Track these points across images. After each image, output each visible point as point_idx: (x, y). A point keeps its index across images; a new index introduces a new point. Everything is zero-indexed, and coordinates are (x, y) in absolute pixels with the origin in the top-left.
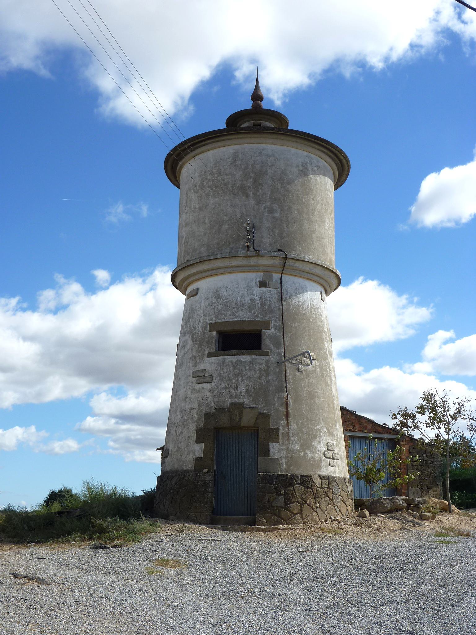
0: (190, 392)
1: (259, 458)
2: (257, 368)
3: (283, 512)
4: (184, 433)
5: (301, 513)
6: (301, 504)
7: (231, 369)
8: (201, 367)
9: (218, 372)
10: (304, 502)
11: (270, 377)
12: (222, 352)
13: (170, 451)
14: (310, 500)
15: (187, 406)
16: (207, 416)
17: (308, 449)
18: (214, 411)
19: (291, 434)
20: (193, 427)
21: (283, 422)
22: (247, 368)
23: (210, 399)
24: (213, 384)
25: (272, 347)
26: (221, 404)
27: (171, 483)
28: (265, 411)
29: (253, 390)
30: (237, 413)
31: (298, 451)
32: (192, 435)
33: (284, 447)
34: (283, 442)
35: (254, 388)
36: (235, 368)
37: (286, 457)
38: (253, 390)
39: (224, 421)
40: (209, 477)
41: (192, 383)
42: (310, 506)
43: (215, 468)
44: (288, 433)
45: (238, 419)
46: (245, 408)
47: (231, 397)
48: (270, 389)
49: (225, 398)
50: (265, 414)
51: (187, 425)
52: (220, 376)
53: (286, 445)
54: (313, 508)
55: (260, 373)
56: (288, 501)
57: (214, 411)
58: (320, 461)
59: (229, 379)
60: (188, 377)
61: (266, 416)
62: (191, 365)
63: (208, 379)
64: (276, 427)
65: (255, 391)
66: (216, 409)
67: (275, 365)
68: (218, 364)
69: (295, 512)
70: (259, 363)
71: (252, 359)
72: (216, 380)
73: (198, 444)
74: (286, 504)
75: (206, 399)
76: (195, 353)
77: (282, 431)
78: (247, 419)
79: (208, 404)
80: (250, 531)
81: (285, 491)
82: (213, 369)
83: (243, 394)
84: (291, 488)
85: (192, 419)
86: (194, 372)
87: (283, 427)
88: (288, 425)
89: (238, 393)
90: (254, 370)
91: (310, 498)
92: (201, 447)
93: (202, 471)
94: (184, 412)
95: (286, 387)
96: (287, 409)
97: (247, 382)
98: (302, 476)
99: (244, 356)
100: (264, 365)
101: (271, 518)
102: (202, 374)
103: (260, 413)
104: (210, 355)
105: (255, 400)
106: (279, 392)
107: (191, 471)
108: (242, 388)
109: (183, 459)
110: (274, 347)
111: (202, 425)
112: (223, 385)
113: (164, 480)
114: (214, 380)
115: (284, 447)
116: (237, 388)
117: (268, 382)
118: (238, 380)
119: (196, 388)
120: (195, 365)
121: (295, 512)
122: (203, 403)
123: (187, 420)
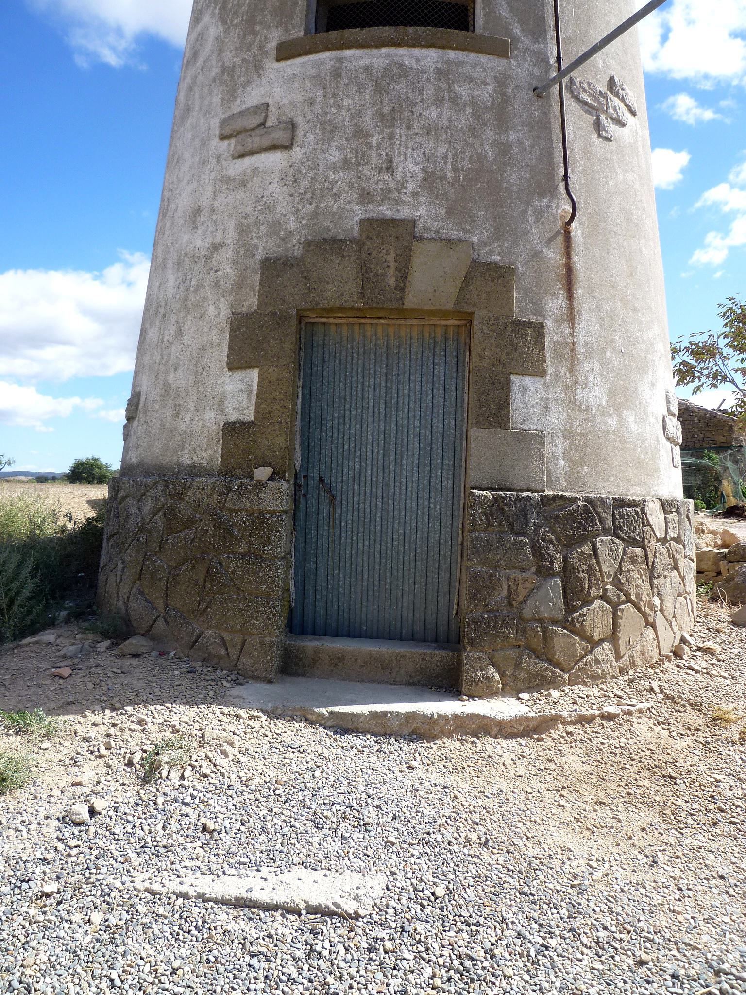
0: (209, 190)
1: (473, 432)
2: (465, 97)
3: (562, 641)
4: (188, 335)
5: (613, 637)
6: (615, 607)
7: (367, 95)
8: (252, 96)
9: (317, 109)
10: (623, 598)
11: (513, 136)
12: (334, 35)
13: (143, 398)
14: (638, 586)
15: (198, 243)
16: (273, 268)
17: (629, 408)
18: (298, 251)
19: (581, 349)
20: (218, 311)
21: (556, 303)
22: (429, 91)
23: (283, 205)
24: (297, 153)
25: (518, 31)
26: (328, 224)
27: (140, 509)
28: (496, 258)
29: (450, 175)
30: (391, 258)
31: (603, 411)
32: (215, 339)
33: (559, 393)
34: (557, 373)
35: (455, 169)
36: (380, 90)
37: (568, 433)
38: (450, 175)
39: (340, 283)
40: (276, 497)
41: (218, 158)
42: (639, 609)
43: (297, 463)
44: (573, 344)
45: (392, 281)
46: (421, 239)
47: (365, 196)
48: (514, 177)
49: (341, 203)
50: (496, 266)
51: (198, 305)
52: (323, 124)
53: (566, 387)
54: (645, 615)
55: (476, 115)
56: (574, 595)
57: (298, 251)
58: (657, 450)
59: (360, 133)
60: (204, 143)
61: (500, 275)
62: (217, 99)
63: (280, 136)
64: (533, 318)
65: (456, 178)
66: (308, 244)
67: (526, 95)
68: (318, 79)
69: (597, 637)
70: (470, 80)
71: (449, 63)
72: (308, 139)
73: (239, 375)
74: (570, 608)
75: (268, 209)
76: (229, 57)
77: (553, 334)
78: (430, 281)
79: (275, 226)
80: (449, 735)
81: (565, 558)
82: (298, 97)
83: (411, 186)
84: (587, 549)
85: (217, 284)
86: (224, 122)
87: (558, 321)
88: (571, 315)
89: (393, 185)
90: (455, 100)
91: (636, 576)
92: (249, 385)
93: (250, 476)
94: (187, 263)
95: (566, 178)
96: (568, 256)
97: (428, 144)
98: (620, 503)
99: (416, 51)
100: (490, 89)
101: (518, 666)
102: (256, 120)
103: (475, 263)
104: (287, 51)
105: (457, 210)
106: (542, 195)
107: (209, 474)
108: (409, 167)
109: (181, 426)
110: (523, 30)
111: (251, 302)
112: (335, 155)
113: (119, 496)
114: (299, 138)
115: (559, 393)
116: (390, 166)
117: (505, 149)
118: (391, 136)
119: (231, 173)
120: (231, 95)
121: (597, 637)
122: (258, 223)
123: (200, 287)
